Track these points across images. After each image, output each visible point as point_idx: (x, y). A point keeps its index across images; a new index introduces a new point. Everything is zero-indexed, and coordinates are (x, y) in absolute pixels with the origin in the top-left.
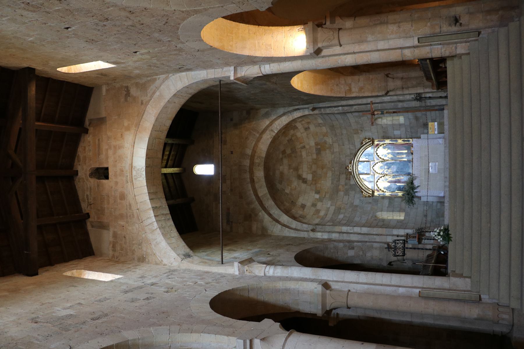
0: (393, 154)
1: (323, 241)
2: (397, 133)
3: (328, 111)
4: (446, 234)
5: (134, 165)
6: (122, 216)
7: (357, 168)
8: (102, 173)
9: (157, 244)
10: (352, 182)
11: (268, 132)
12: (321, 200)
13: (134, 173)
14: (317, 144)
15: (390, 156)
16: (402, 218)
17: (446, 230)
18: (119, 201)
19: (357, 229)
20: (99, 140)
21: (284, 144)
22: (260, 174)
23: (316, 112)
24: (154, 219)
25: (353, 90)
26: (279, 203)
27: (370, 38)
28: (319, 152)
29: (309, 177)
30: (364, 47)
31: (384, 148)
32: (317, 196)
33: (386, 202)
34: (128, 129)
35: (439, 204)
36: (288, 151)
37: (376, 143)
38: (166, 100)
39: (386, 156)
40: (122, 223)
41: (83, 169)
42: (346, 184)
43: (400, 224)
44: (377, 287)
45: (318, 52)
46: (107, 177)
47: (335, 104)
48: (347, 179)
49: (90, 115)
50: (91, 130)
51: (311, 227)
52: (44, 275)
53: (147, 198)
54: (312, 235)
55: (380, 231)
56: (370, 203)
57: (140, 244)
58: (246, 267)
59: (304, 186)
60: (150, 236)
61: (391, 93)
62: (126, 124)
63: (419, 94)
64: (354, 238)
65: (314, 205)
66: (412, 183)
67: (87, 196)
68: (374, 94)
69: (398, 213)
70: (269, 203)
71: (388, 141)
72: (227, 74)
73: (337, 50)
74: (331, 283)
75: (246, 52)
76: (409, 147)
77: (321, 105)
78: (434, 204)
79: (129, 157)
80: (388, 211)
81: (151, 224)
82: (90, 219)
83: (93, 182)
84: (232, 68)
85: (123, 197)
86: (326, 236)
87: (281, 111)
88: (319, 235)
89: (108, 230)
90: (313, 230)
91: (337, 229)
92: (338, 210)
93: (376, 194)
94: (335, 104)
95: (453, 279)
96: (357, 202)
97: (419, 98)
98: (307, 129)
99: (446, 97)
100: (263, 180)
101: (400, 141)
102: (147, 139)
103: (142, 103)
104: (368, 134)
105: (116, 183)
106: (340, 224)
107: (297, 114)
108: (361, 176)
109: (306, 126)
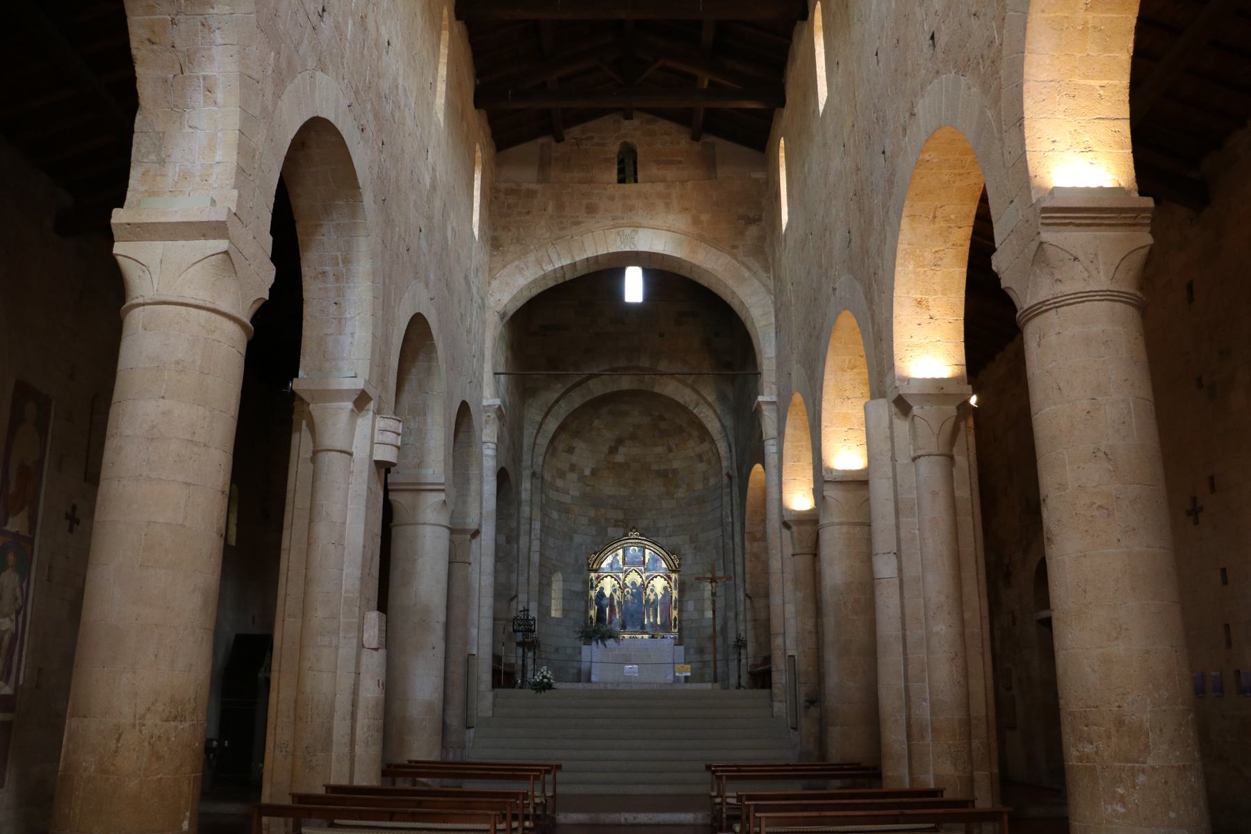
0: (655, 601)
1: (519, 493)
2: (690, 606)
3: (726, 499)
4: (543, 687)
5: (640, 230)
6: (560, 207)
7: (633, 544)
8: (627, 169)
9: (521, 271)
10: (611, 531)
11: (695, 397)
12: (582, 478)
13: (628, 231)
14: (675, 471)
15: (652, 597)
16: (553, 614)
17: (549, 686)
18: (585, 202)
19: (536, 545)
20: (680, 162)
21: (675, 423)
22: (626, 383)
23: (725, 480)
24: (558, 265)
25: (756, 545)
26: (575, 414)
27: (800, 595)
28: (663, 474)
29: (619, 458)
30: (789, 586)
31: (665, 588)
32: (587, 472)
33: (578, 587)
34: (696, 221)
35: (575, 671)
36: (663, 425)
37: (673, 576)
38: (735, 289)
39: (652, 591)
40: (550, 208)
41: (633, 130)
42: (607, 520)
43: (544, 610)
44: (476, 601)
45: (786, 525)
46: (621, 181)
47: (736, 513)
48: (616, 521)
49: (723, 146)
50: (697, 147)
51: (538, 470)
52: (476, 119)
53: (590, 253)
54: (526, 473)
55: (535, 580)
56: (577, 561)
57: (518, 241)
58: (493, 415)
59: (605, 449)
60: (531, 258)
61: (748, 602)
62: (704, 217)
63: (745, 646)
64: (523, 541)
65: (573, 468)
66: (610, 637)
67: (591, 138)
68: (747, 576)
69: (560, 606)
70: (577, 400)
71: (675, 594)
72: (766, 390)
73: (789, 551)
74: (478, 539)
75: (789, 431)
76: (666, 627)
77: (735, 489)
78: (575, 664)
79: (651, 223)
80: (564, 591)
81: (551, 262)
82: (553, 143)
83: (614, 149)
84: (774, 398)
85: (591, 210)
86: (525, 496)
87: (729, 423)
88: (526, 485)
89: (538, 182)
90: (534, 474)
91: (537, 513)
92: (564, 509)
93: (593, 575)
94: (736, 513)
95: (490, 696)
96: (578, 539)
97: (740, 644)
98: (700, 457)
99: (739, 686)
100: (615, 389)
101: (675, 613)
102: (678, 255)
103: (734, 247)
104: (689, 558)
105: (612, 198)
106: (544, 514)
107: (722, 447)
108: (620, 552)
109: (705, 458)
